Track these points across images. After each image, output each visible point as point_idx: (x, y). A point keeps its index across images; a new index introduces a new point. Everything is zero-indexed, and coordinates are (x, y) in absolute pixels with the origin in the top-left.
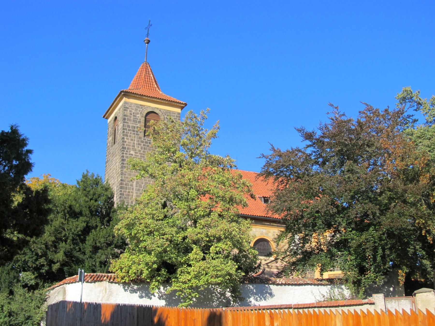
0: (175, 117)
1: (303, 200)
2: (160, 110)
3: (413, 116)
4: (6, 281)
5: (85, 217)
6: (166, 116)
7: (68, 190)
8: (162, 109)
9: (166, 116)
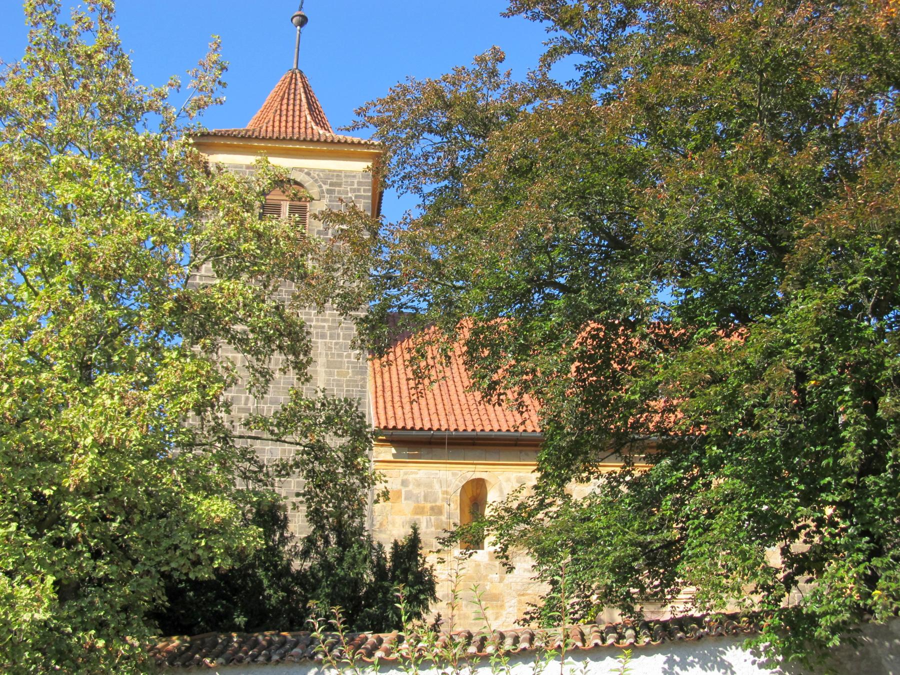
0: (356, 186)
1: (182, 614)
2: (308, 174)
3: (534, 471)
4: (81, 451)
5: (648, 616)
6: (325, 187)
7: (326, 453)
8: (315, 170)
9: (325, 187)
